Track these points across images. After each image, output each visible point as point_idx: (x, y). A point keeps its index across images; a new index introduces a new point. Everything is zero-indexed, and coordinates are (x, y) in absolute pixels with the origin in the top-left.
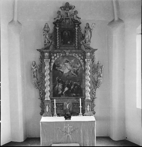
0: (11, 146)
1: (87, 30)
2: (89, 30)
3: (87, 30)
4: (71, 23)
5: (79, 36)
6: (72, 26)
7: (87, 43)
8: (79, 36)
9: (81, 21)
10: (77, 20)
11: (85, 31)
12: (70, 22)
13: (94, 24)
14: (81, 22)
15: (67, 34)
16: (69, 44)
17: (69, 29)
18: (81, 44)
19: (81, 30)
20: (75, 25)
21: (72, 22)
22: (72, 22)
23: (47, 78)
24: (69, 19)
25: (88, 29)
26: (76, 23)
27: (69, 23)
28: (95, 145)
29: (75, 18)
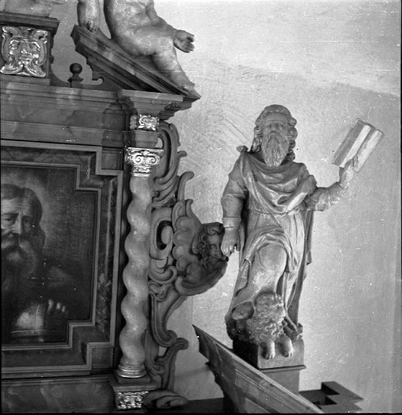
0: (33, 412)
1: (275, 197)
2: (296, 200)
3: (275, 197)
4: (74, 81)
5: (162, 247)
6: (82, 124)
7: (273, 351)
8: (162, 247)
9: (187, 66)
10: (152, 58)
11: (245, 200)
12: (64, 74)
13: (366, 129)
14: (198, 90)
15: (13, 217)
16: (33, 339)
17: (39, 161)
18: (171, 334)
19: (190, 175)
20: (127, 111)
21: (86, 74)
22: (86, 74)
23: (257, 242)
24: (53, 32)
25: (289, 185)
26: (136, 95)
27: (54, 82)
28: (8, 365)
29: (125, 32)
